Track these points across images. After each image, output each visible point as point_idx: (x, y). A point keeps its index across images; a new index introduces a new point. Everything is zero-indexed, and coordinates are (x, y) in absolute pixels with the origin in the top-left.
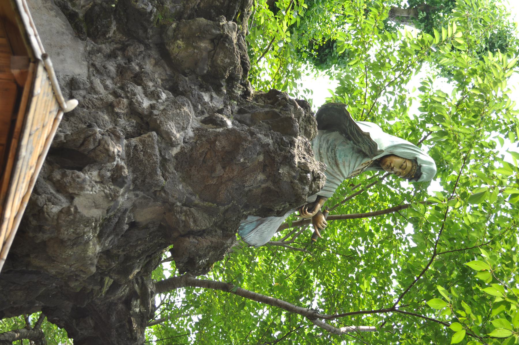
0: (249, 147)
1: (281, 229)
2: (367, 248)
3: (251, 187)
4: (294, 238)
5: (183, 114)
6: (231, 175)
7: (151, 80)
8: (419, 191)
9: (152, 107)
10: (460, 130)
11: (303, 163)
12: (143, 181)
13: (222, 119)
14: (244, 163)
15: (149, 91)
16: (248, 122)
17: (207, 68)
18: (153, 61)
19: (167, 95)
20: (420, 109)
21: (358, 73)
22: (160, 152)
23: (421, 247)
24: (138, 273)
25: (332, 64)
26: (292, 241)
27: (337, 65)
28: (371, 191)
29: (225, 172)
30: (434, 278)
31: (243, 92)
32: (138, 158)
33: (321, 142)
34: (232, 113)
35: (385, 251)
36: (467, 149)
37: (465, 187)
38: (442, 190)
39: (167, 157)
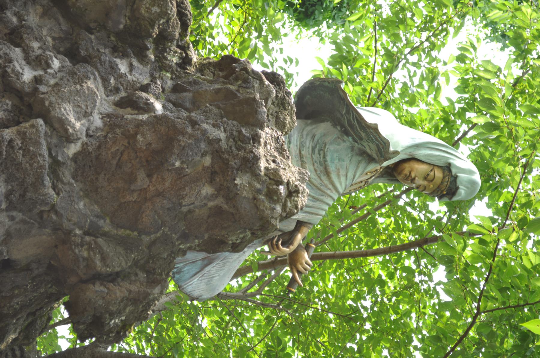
0: (189, 144)
1: (240, 273)
2: (375, 303)
3: (192, 206)
4: (261, 288)
5: (86, 91)
6: (160, 188)
7: (36, 39)
8: (454, 217)
9: (37, 80)
10: (517, 122)
11: (273, 169)
12: (23, 196)
13: (147, 100)
14: (181, 169)
15: (33, 55)
16: (188, 105)
17: (124, 22)
18: (40, 10)
19: (60, 63)
20: (457, 89)
21: (363, 34)
22: (50, 150)
23: (459, 301)
24: (15, 340)
25: (324, 19)
26: (259, 292)
27: (330, 21)
28: (381, 215)
29: (151, 182)
30: (476, 349)
31: (180, 58)
32: (15, 160)
33: (302, 138)
34: (163, 91)
35: (404, 307)
36: (528, 152)
37: (524, 210)
38: (491, 215)
39: (60, 158)
